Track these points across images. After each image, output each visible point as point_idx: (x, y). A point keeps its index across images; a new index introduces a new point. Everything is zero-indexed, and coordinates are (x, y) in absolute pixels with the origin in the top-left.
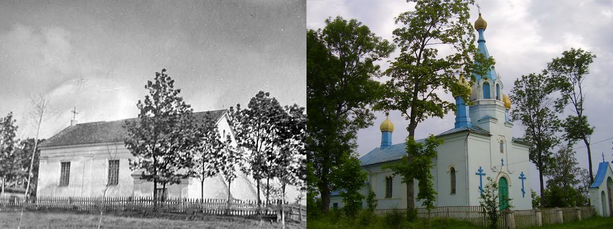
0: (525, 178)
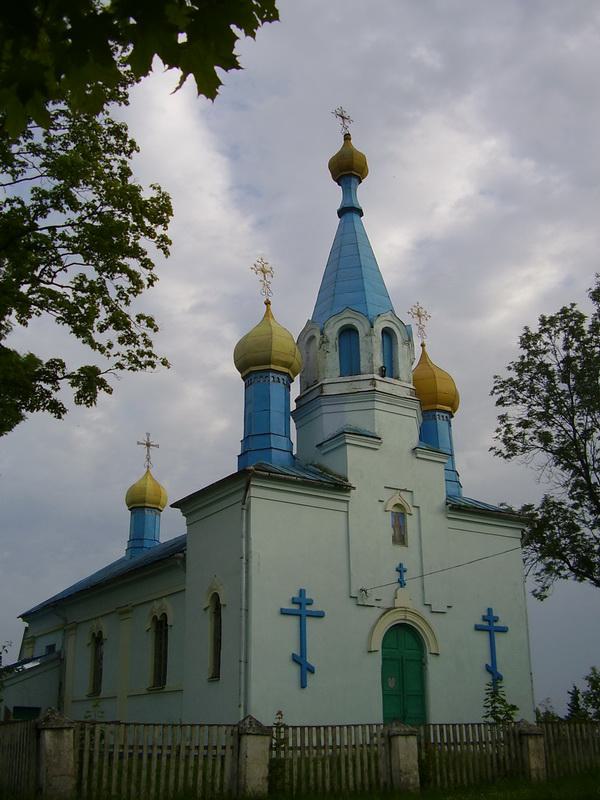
0: (504, 630)
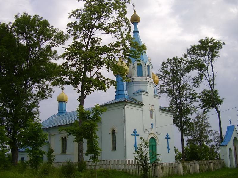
0: (170, 138)
